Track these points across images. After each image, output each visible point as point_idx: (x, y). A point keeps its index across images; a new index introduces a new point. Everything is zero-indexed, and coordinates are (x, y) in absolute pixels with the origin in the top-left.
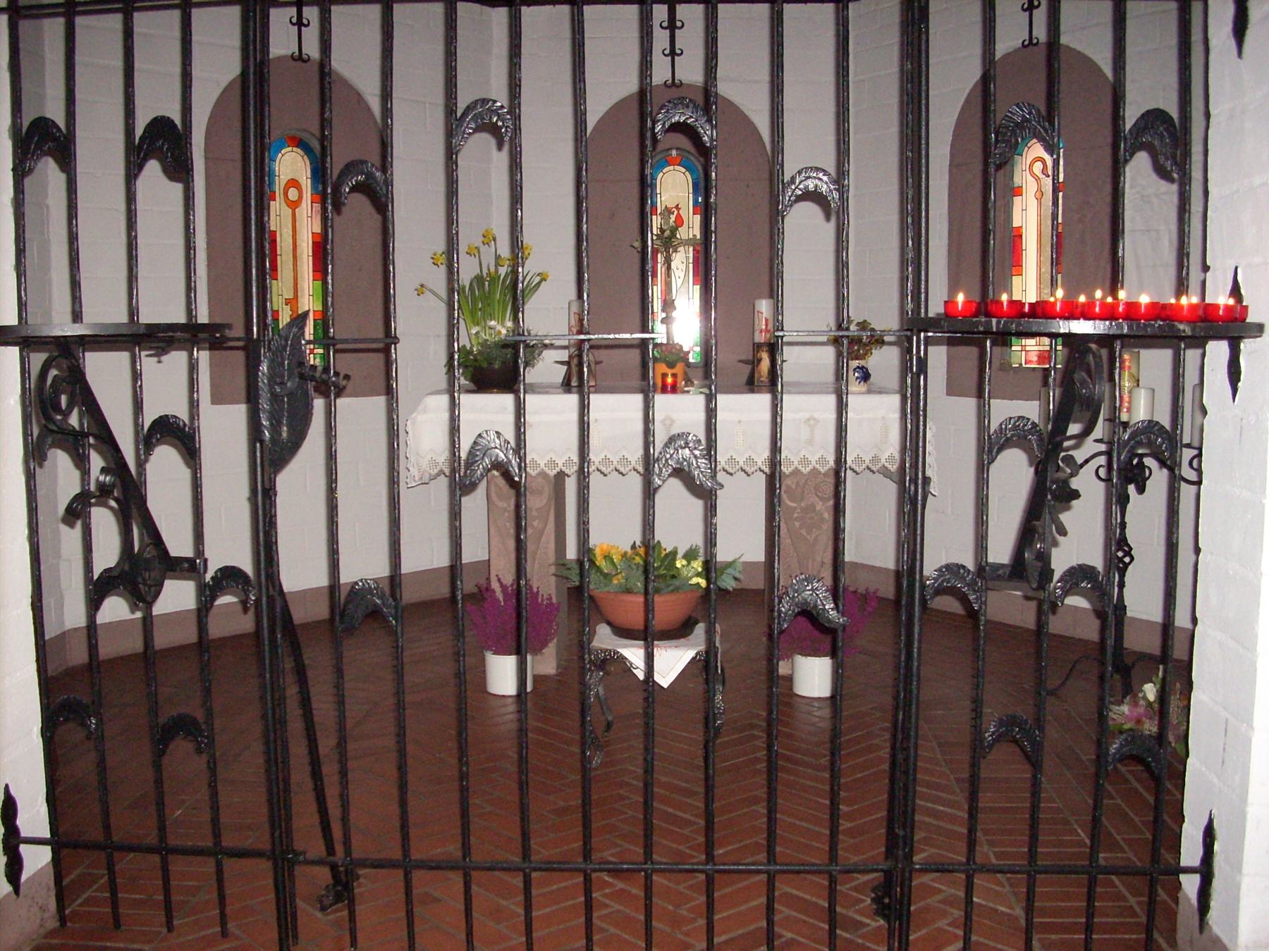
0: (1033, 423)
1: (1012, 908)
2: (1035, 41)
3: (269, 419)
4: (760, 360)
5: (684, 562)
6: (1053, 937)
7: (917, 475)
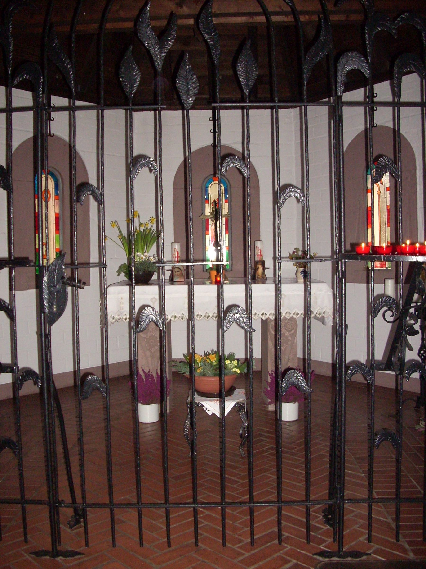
0: (393, 299)
1: (387, 518)
2: (375, 125)
3: (48, 303)
4: (258, 269)
5: (229, 362)
6: (407, 532)
7: (342, 324)
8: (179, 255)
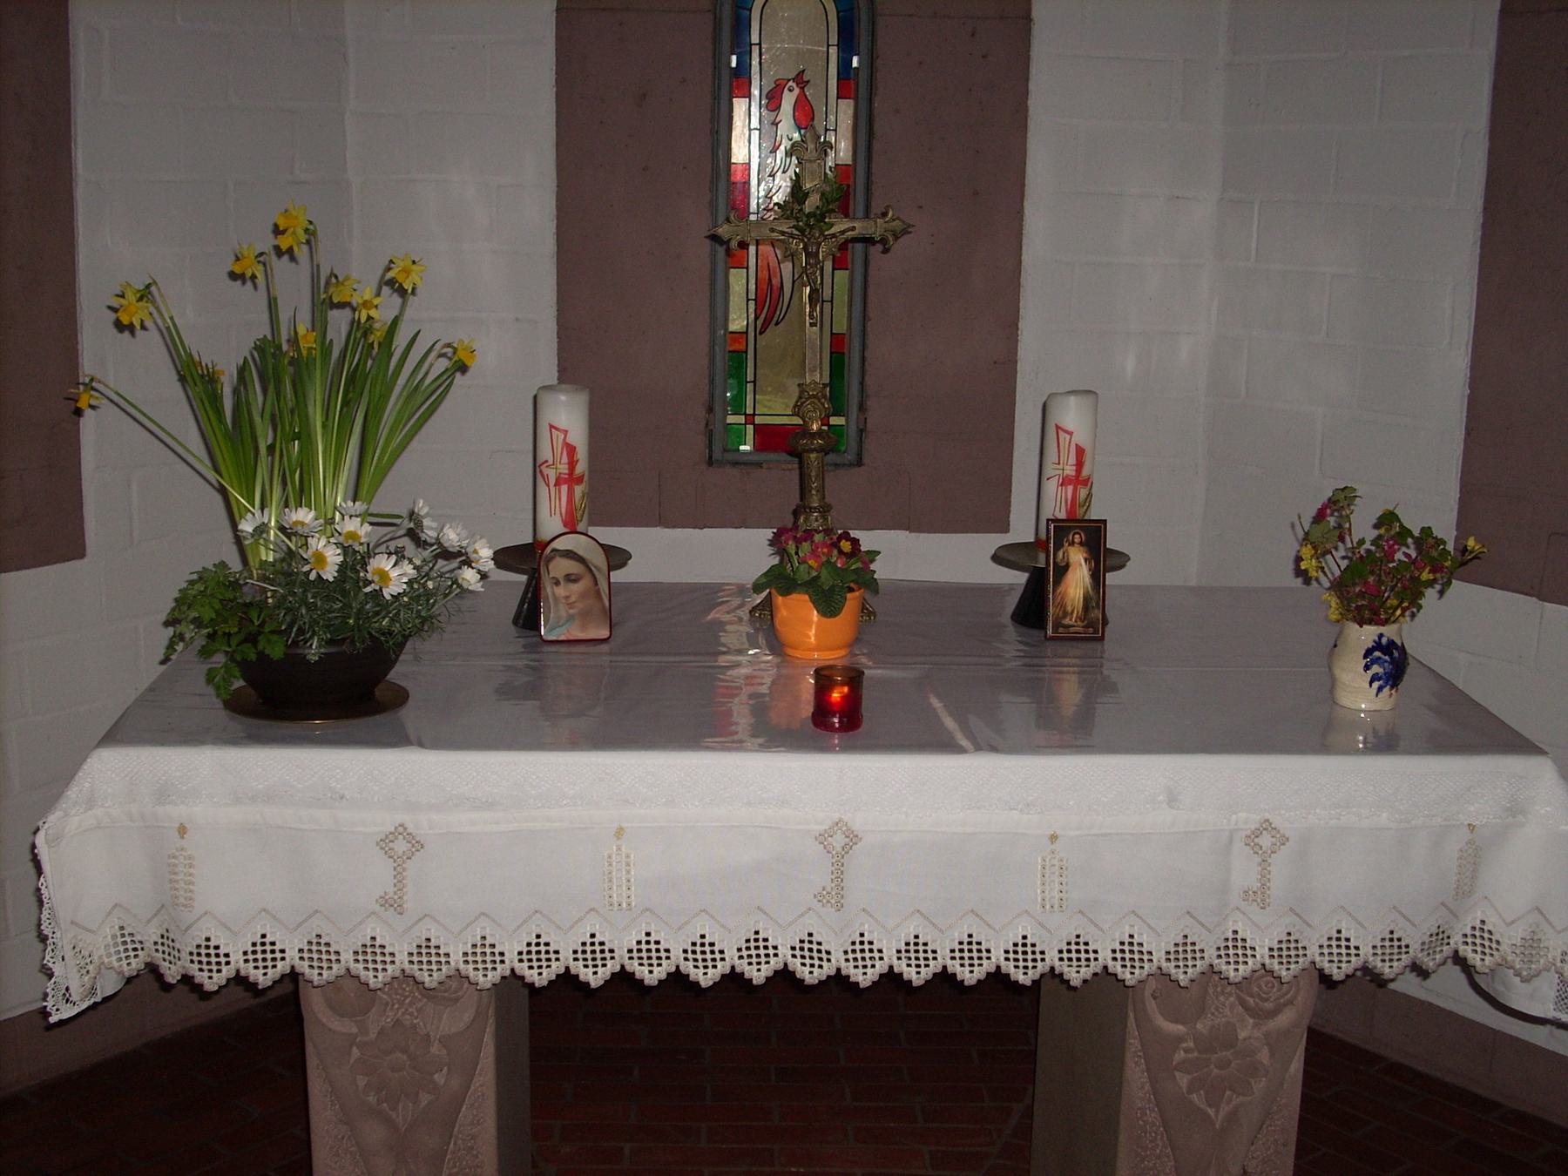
4: (1062, 570)
8: (581, 467)
